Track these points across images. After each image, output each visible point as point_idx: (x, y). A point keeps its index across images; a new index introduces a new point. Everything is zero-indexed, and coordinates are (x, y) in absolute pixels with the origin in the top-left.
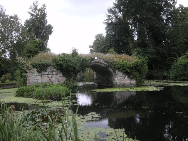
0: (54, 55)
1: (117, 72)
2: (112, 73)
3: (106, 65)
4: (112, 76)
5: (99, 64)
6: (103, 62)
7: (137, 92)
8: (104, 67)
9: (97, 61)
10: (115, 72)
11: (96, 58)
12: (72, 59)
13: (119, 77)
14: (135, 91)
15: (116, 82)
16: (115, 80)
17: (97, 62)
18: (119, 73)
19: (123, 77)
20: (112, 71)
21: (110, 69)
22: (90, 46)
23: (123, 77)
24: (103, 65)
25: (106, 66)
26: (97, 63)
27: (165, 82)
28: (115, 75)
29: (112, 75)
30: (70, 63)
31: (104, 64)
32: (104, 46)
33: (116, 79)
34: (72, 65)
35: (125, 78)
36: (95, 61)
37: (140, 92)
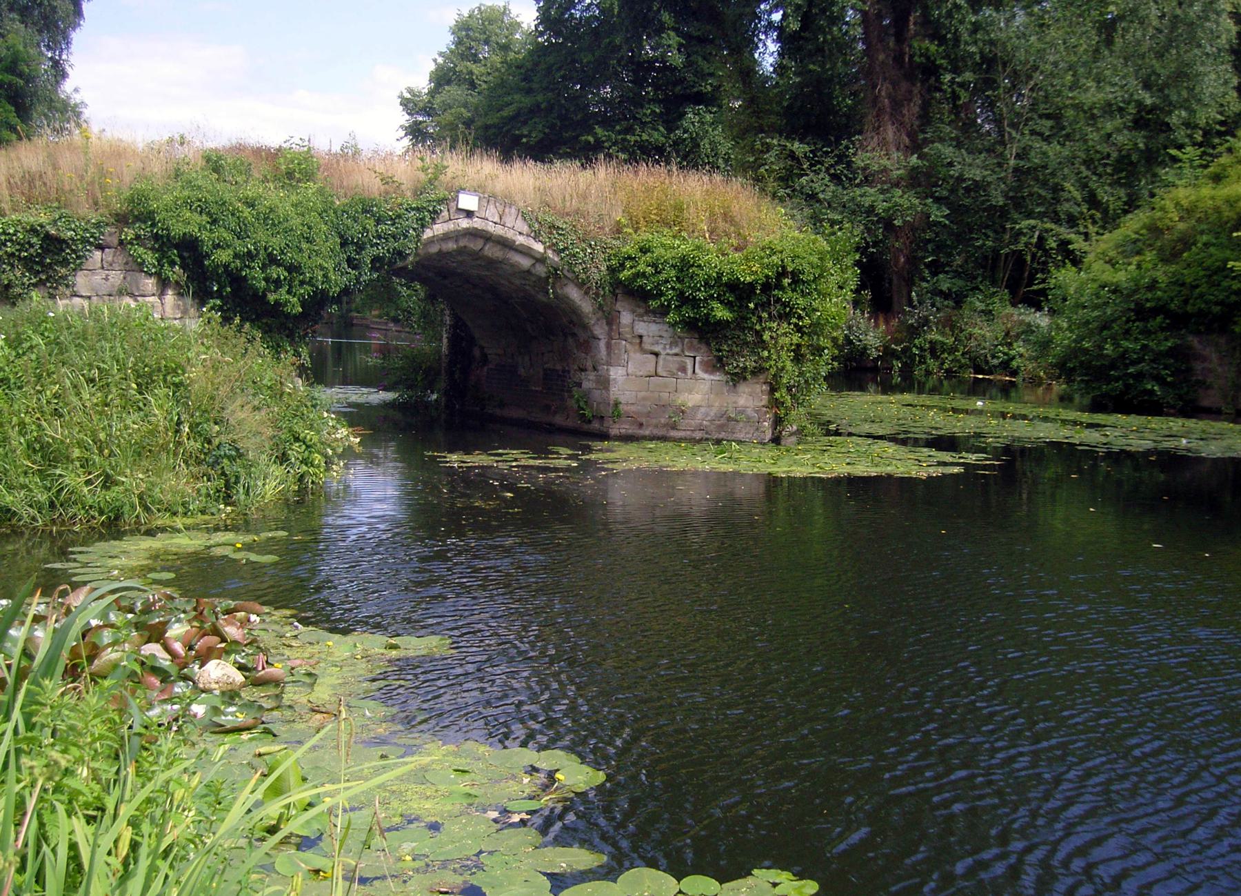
0: (119, 152)
1: (626, 318)
2: (585, 327)
3: (542, 260)
4: (587, 345)
5: (491, 251)
6: (516, 230)
7: (772, 481)
8: (528, 272)
9: (477, 223)
10: (611, 320)
11: (468, 201)
12: (275, 197)
13: (637, 357)
14: (706, 475)
15: (612, 397)
16: (605, 383)
17: (473, 234)
18: (642, 328)
19: (673, 363)
20: (586, 306)
21: (574, 293)
22: (410, 91)
23: (673, 363)
24: (525, 263)
25: (541, 270)
26: (475, 245)
27: (1075, 423)
28: (609, 346)
29: (587, 342)
30: (261, 236)
31: (526, 252)
32: (522, 101)
33: (616, 373)
34: (276, 243)
35: (683, 369)
36: (464, 223)
37: (794, 483)
